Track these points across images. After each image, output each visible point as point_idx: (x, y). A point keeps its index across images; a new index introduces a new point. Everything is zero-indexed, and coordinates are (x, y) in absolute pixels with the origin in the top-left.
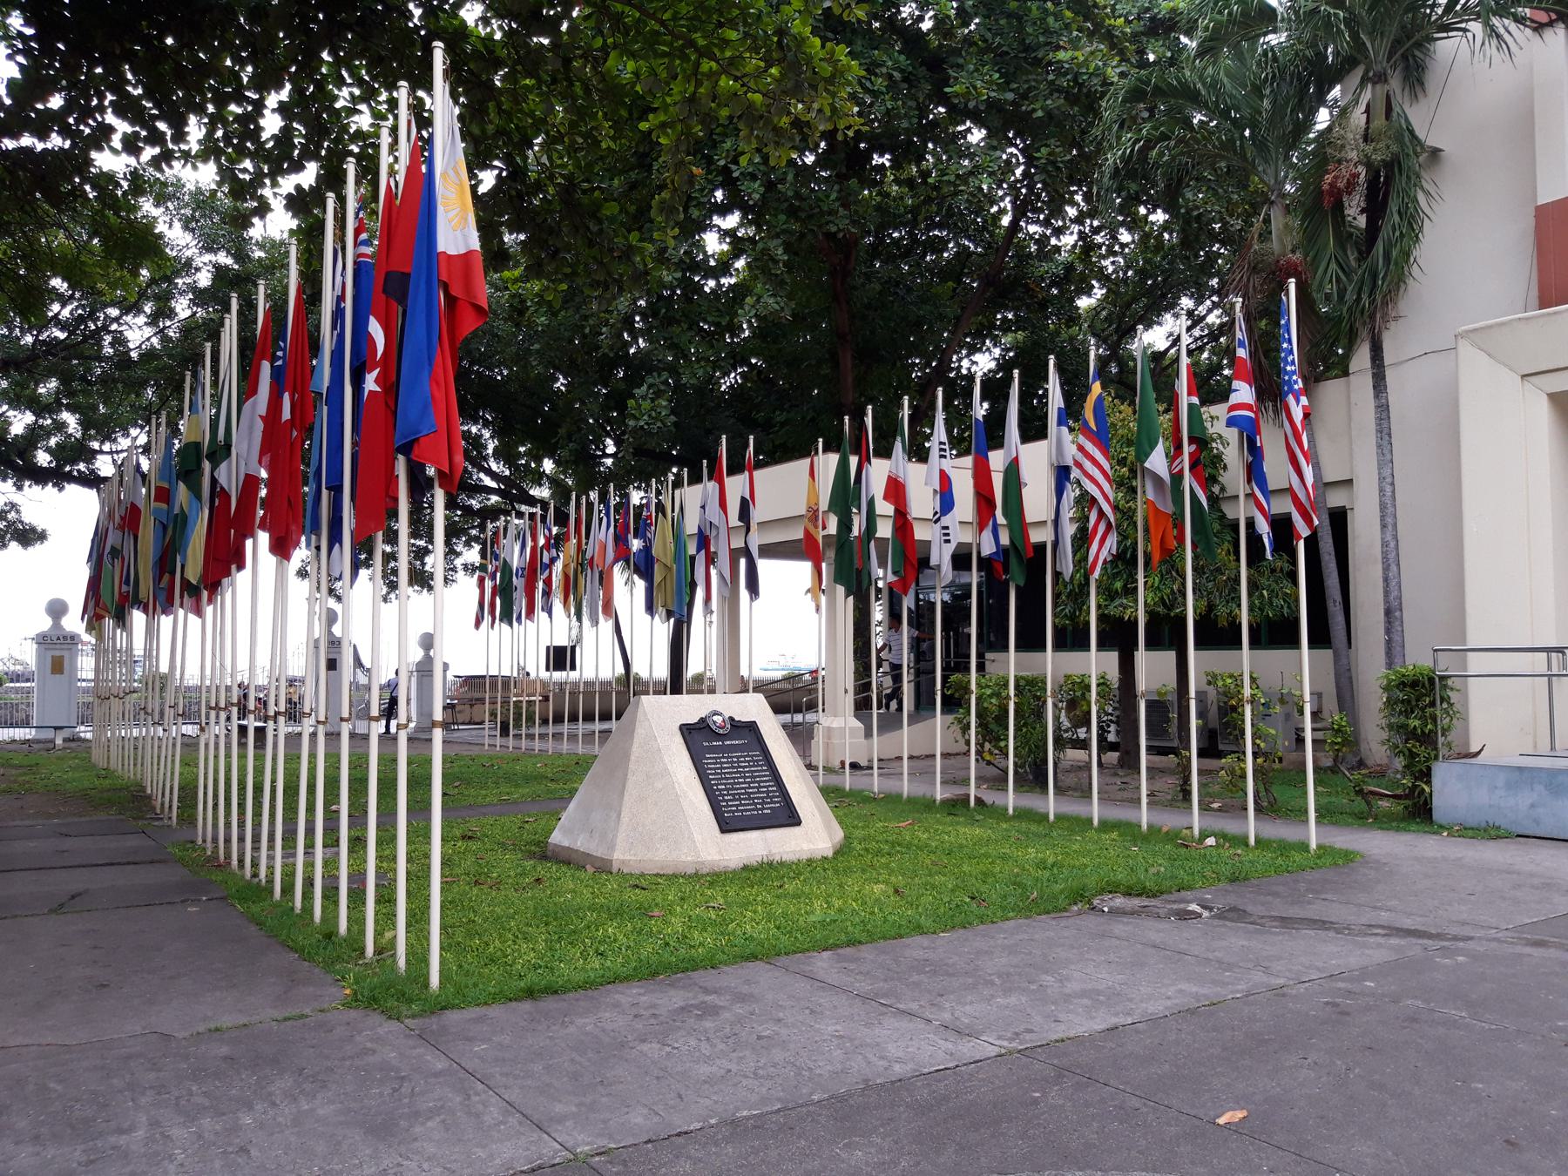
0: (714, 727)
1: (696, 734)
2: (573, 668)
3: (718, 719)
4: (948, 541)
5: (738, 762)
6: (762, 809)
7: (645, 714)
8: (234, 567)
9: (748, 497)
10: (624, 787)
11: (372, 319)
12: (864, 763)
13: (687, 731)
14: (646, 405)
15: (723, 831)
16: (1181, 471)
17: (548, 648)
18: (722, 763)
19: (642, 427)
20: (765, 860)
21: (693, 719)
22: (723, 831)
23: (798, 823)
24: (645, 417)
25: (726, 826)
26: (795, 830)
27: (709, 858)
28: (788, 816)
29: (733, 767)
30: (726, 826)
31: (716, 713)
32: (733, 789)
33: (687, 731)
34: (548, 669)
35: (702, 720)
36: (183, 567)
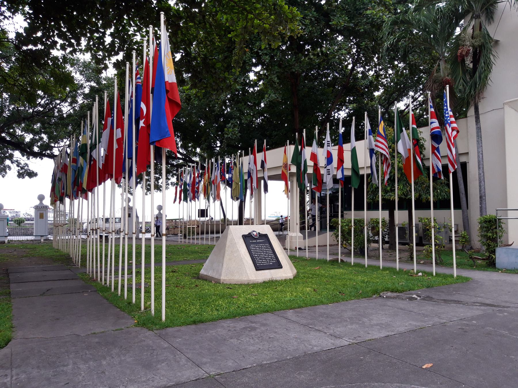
1: (248, 238)
3: (255, 233)
4: (329, 174)
9: (264, 160)
10: (224, 255)
12: (303, 248)
13: (245, 237)
15: (257, 270)
18: (256, 248)
19: (229, 137)
21: (246, 233)
22: (257, 270)
25: (258, 268)
27: (252, 279)
30: (258, 268)
31: (254, 231)
32: (260, 256)
33: (245, 237)
34: (199, 217)
35: (250, 234)
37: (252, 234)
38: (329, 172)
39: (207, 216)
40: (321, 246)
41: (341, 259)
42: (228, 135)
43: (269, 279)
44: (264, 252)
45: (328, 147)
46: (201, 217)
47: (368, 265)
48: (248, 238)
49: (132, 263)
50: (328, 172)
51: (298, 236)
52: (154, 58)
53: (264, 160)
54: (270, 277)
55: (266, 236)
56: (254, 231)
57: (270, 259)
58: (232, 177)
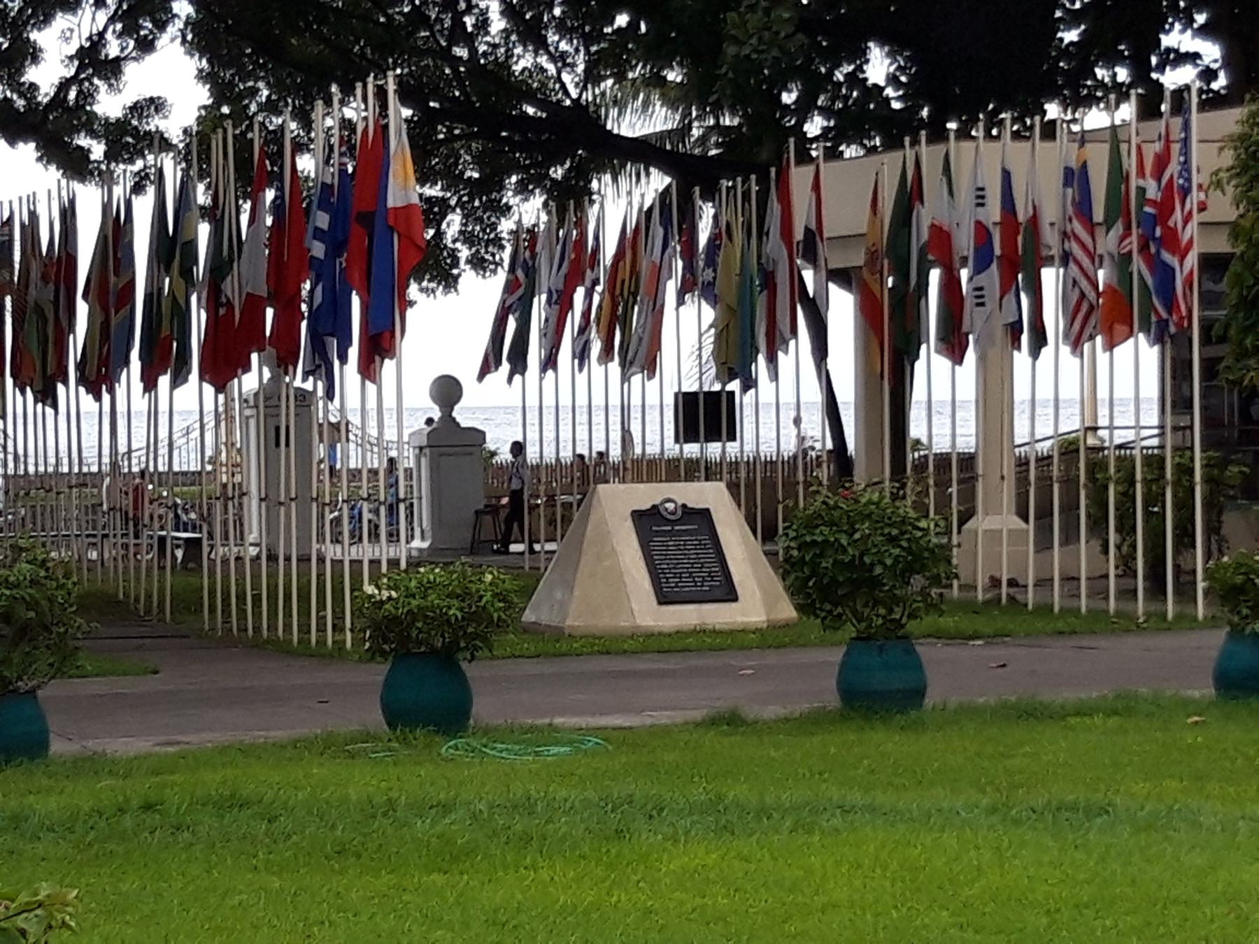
0: (664, 513)
1: (647, 520)
2: (732, 437)
3: (670, 506)
4: (982, 304)
5: (685, 545)
6: (702, 586)
7: (599, 500)
8: (240, 371)
9: (813, 226)
10: (579, 561)
11: (354, 292)
12: (1021, 582)
13: (638, 516)
14: (754, 19)
15: (660, 603)
16: (1130, 252)
17: (676, 395)
18: (668, 546)
19: (747, 57)
20: (698, 628)
21: (646, 506)
22: (660, 603)
23: (735, 599)
24: (754, 41)
25: (664, 598)
26: (733, 605)
27: (644, 624)
28: (730, 595)
29: (680, 550)
30: (664, 598)
31: (669, 500)
32: (674, 568)
33: (638, 516)
34: (677, 440)
35: (654, 507)
36: (663, 674)
37: (661, 508)
38: (982, 296)
39: (732, 437)
40: (1094, 578)
41: (1008, 595)
42: (741, 43)
43: (692, 627)
44: (689, 559)
45: (980, 209)
46: (686, 441)
47: (1061, 609)
48: (647, 520)
49: (325, 617)
50: (977, 297)
51: (1010, 531)
52: (362, 141)
53: (813, 226)
54: (697, 622)
55: (704, 515)
56: (669, 500)
57: (703, 577)
58: (715, 278)
